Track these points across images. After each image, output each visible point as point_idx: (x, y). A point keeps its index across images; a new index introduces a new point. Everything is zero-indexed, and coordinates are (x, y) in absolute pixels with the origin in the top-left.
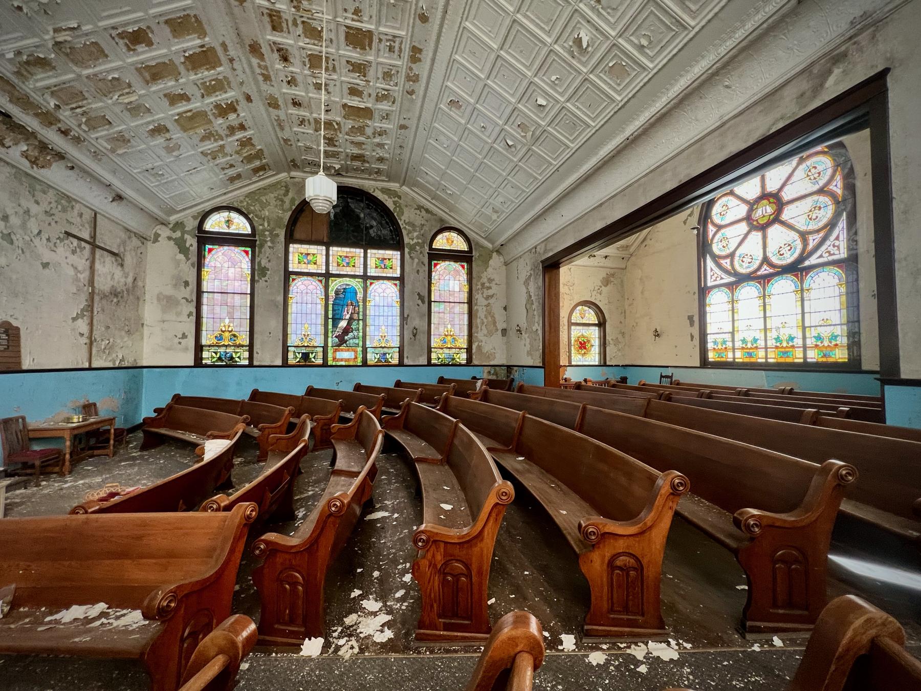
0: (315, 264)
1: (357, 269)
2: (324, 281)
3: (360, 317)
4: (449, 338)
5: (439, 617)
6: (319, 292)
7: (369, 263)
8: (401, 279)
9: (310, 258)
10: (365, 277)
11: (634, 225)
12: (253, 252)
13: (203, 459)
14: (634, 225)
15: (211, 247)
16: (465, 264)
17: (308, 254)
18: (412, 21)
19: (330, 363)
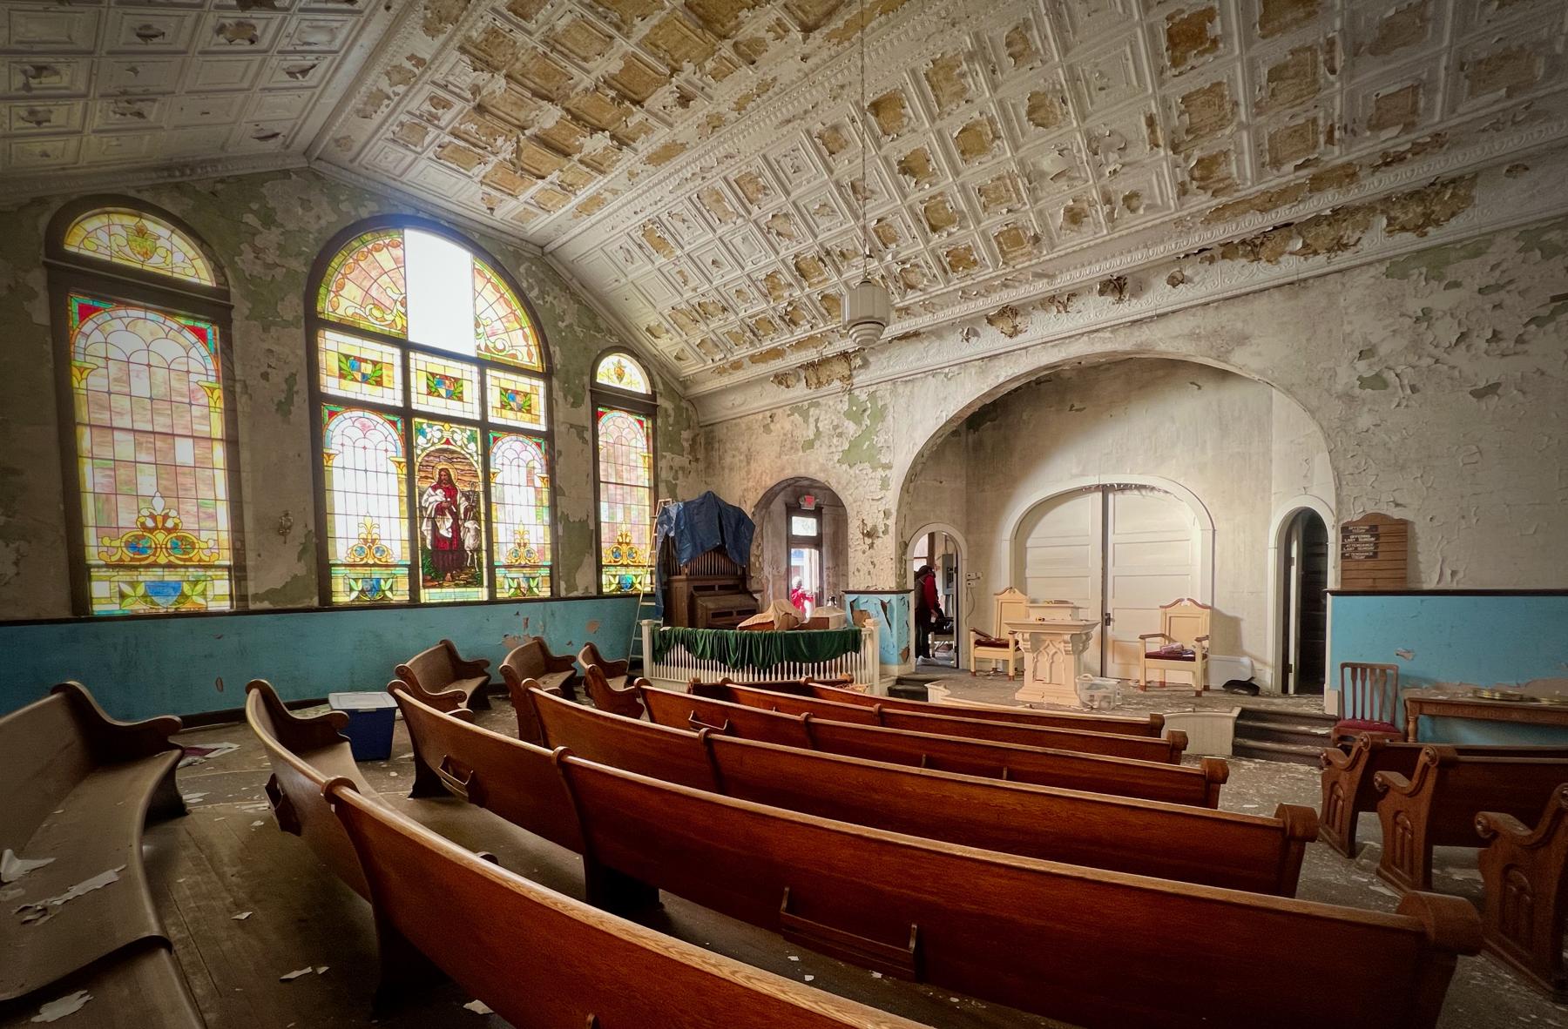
0: (529, 412)
1: (468, 407)
2: (332, 408)
3: (481, 507)
4: (160, 537)
5: (907, 946)
6: (391, 447)
7: (413, 383)
8: (549, 436)
9: (519, 399)
10: (484, 426)
11: (330, 6)
12: (226, 339)
13: (1244, 714)
14: (330, 6)
15: (88, 301)
16: (211, 331)
17: (517, 392)
18: (1483, 112)
19: (563, 594)
